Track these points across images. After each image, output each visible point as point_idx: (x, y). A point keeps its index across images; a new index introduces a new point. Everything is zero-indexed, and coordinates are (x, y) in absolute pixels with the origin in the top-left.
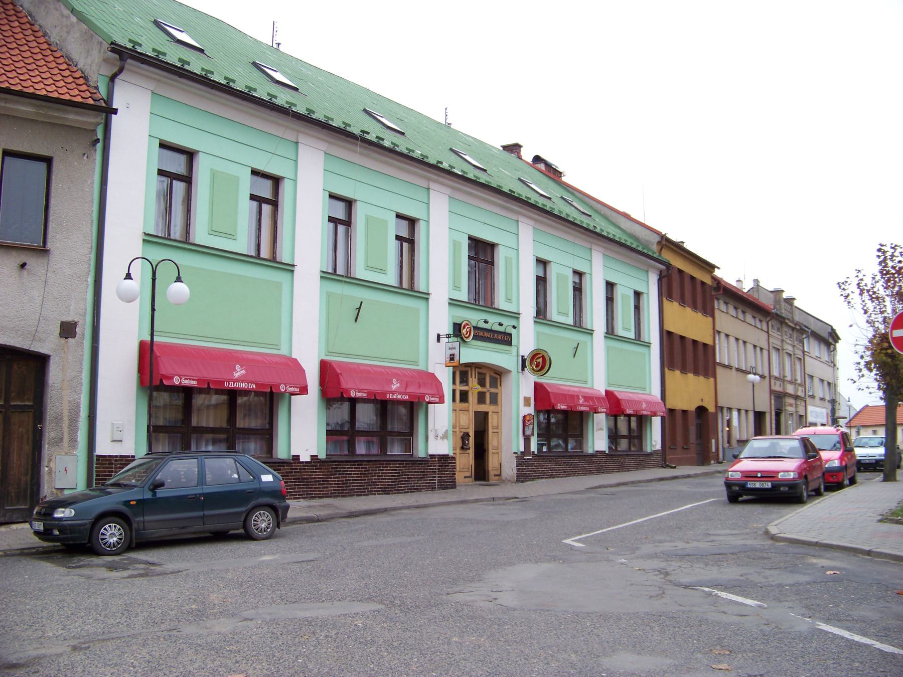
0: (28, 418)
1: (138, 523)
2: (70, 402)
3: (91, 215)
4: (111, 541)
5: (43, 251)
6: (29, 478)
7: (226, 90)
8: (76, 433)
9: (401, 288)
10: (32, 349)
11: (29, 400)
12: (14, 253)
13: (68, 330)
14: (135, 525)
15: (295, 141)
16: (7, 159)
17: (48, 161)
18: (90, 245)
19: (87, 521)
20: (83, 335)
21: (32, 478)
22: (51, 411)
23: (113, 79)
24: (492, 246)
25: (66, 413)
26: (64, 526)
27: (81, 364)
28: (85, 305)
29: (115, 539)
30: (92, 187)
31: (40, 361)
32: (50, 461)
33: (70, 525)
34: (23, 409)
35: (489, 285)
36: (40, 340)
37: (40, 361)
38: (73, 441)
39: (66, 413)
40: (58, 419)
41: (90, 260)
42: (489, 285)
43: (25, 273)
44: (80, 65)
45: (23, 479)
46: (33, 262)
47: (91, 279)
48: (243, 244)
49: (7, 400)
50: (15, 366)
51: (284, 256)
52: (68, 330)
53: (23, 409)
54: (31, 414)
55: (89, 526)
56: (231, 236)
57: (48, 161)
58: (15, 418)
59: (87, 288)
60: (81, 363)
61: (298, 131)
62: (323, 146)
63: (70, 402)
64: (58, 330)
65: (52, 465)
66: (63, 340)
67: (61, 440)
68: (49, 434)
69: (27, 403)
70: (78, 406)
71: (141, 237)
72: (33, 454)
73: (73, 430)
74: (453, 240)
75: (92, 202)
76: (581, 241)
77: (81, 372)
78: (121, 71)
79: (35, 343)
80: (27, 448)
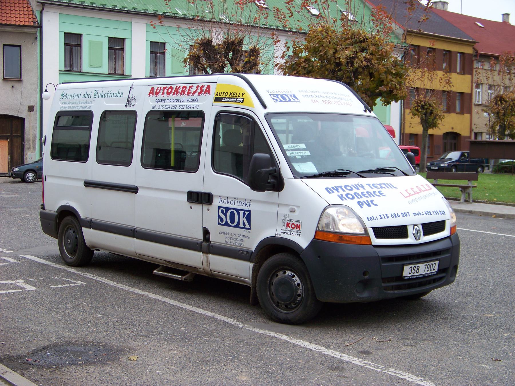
0: (19, 140)
1: (39, 173)
2: (33, 134)
3: (37, 66)
4: (30, 178)
5: (20, 80)
6: (20, 161)
7: (114, 11)
8: (35, 145)
9: (115, 74)
10: (18, 116)
11: (19, 134)
12: (10, 82)
13: (31, 109)
14: (38, 174)
15: (130, 21)
16: (5, 47)
17: (20, 46)
18: (37, 77)
19: (22, 172)
20: (36, 110)
21: (21, 161)
22: (26, 138)
23: (41, 12)
24: (80, 36)
25: (31, 138)
26: (15, 173)
27: (36, 121)
28: (37, 99)
29: (31, 178)
30: (37, 55)
31: (22, 120)
32: (26, 155)
33: (17, 173)
34: (17, 137)
35: (79, 56)
36: (21, 113)
37: (22, 120)
38: (34, 148)
39: (31, 138)
40: (29, 140)
41: (38, 83)
42: (79, 56)
43: (14, 89)
44: (31, 5)
45: (18, 161)
46: (16, 85)
47: (38, 90)
48: (105, 70)
49: (11, 134)
50: (14, 122)
51: (127, 73)
52: (31, 109)
53: (17, 137)
54: (20, 139)
55: (23, 173)
56: (100, 67)
57: (20, 46)
58: (15, 140)
59: (37, 93)
60: (36, 120)
61: (131, 17)
62: (59, 11)
63: (33, 134)
64: (27, 109)
65: (27, 156)
66: (29, 113)
67: (30, 148)
68: (26, 146)
69: (19, 135)
70: (36, 136)
71: (58, 72)
72: (21, 153)
73: (34, 144)
74: (89, 41)
75: (37, 61)
76: (126, 18)
77: (36, 124)
78: (43, 9)
79: (19, 114)
80: (19, 151)
